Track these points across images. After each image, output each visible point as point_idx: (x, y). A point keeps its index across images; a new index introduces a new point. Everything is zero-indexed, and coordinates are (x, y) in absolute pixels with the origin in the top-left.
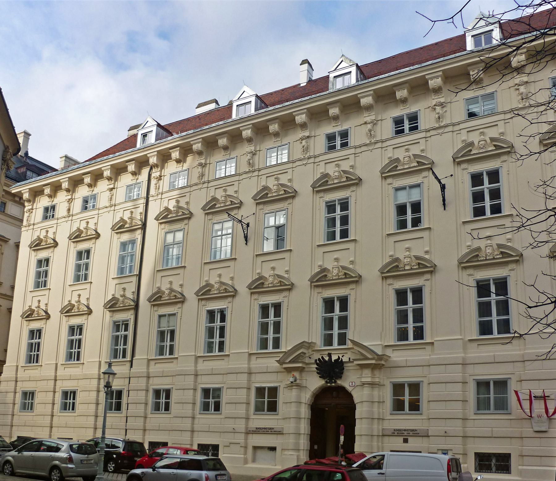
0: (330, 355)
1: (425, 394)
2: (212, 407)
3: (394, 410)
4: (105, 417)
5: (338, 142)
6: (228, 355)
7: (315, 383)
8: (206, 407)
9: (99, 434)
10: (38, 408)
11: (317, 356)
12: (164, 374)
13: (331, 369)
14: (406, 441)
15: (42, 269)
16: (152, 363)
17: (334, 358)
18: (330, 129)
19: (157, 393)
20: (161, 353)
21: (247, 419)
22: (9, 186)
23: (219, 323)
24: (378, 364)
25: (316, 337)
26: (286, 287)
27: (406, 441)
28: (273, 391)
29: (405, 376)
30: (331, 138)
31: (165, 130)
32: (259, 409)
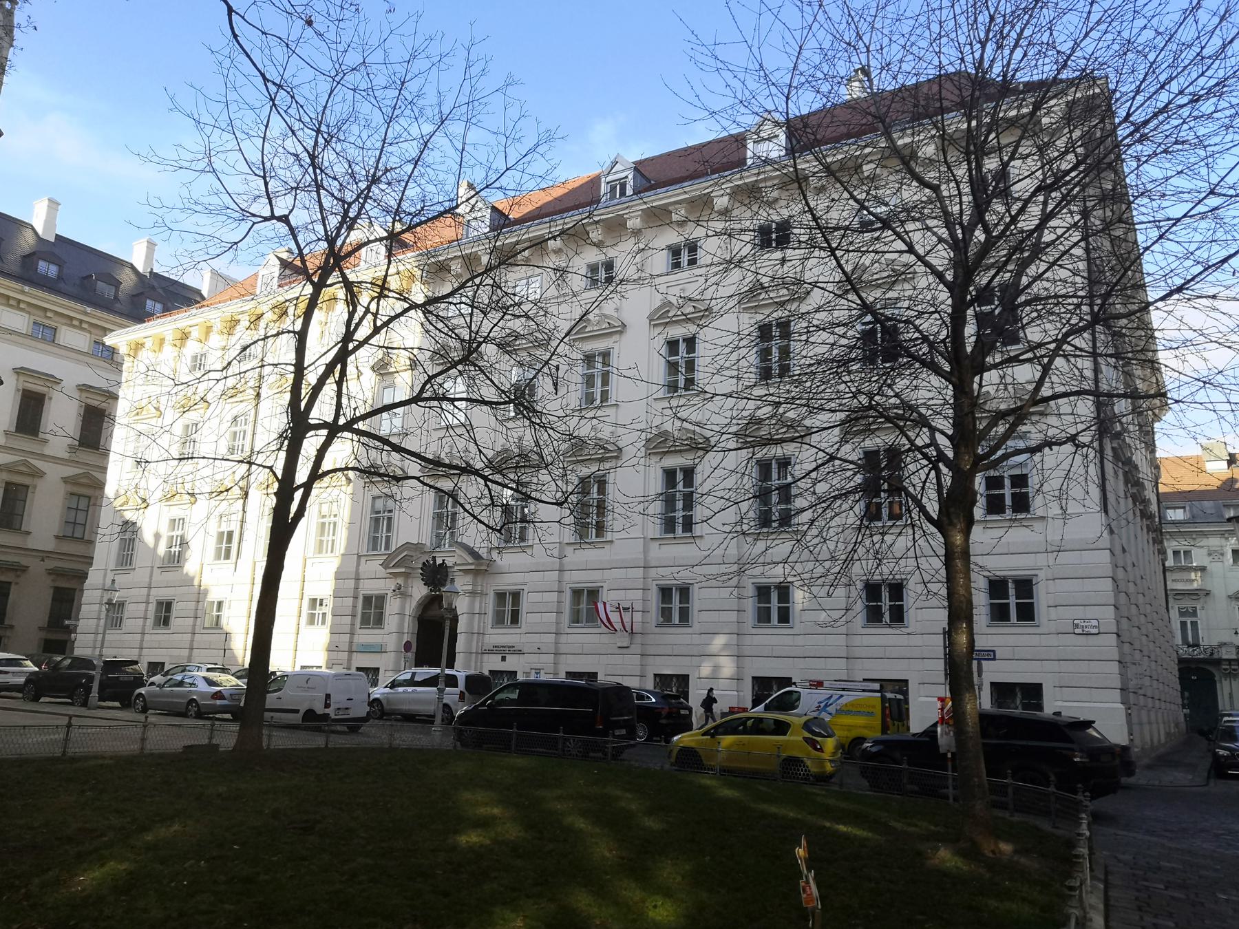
0: (434, 558)
1: (525, 606)
2: (508, 617)
3: (992, 619)
4: (104, 634)
5: (685, 258)
6: (612, 542)
7: (419, 591)
8: (763, 617)
9: (97, 652)
10: (128, 624)
11: (424, 558)
12: (588, 566)
13: (436, 575)
14: (504, 659)
15: (238, 429)
16: (363, 560)
17: (439, 561)
18: (592, 256)
19: (666, 593)
20: (374, 549)
21: (352, 634)
22: (106, 331)
23: (595, 496)
24: (481, 567)
25: (427, 539)
26: (701, 446)
27: (504, 659)
28: (381, 599)
29: (507, 583)
30: (675, 251)
31: (802, 135)
32: (365, 622)
